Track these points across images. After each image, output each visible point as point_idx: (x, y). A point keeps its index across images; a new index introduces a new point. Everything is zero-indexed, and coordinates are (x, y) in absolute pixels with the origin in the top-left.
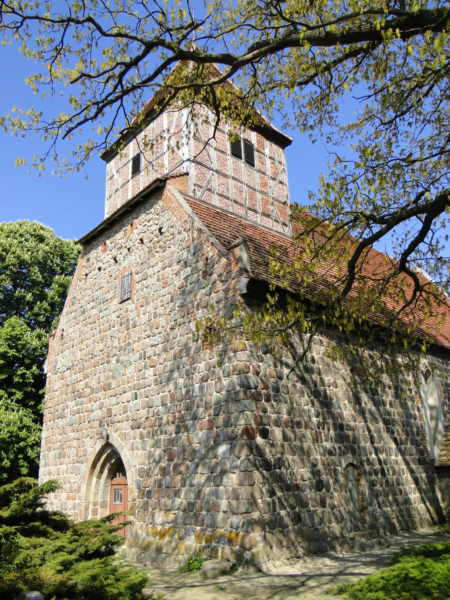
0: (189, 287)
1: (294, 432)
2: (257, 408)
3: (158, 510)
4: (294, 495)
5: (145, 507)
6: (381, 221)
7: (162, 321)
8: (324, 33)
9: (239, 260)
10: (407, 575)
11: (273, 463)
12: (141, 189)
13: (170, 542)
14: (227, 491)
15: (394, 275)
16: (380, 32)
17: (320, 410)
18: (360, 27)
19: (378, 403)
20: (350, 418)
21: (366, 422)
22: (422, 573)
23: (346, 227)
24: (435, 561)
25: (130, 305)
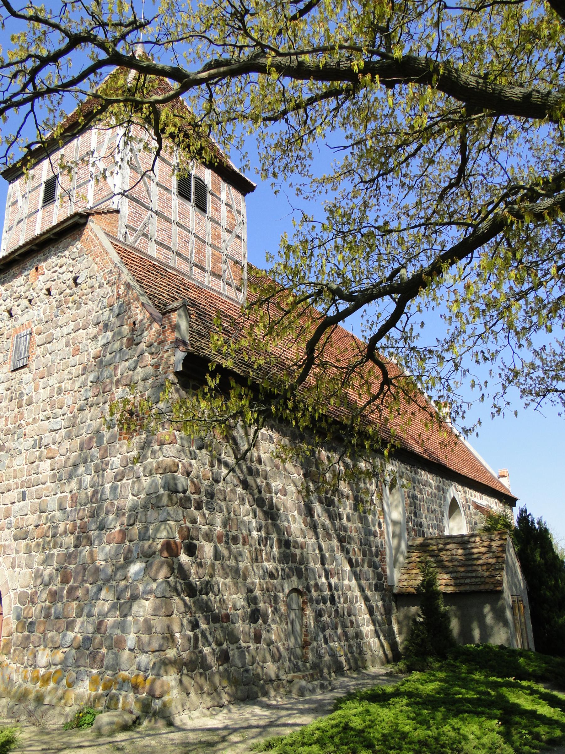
0: (108, 357)
1: (229, 549)
2: (184, 517)
3: (42, 647)
4: (222, 627)
5: (25, 644)
6: (349, 298)
7: (68, 399)
8: (296, 63)
9: (176, 327)
10: (347, 724)
11: (199, 587)
12: (54, 223)
13: (56, 689)
14: (136, 622)
15: (361, 363)
16: (357, 74)
17: (263, 523)
18: (338, 63)
19: (334, 516)
20: (298, 533)
21: (317, 538)
22: (364, 722)
23: (309, 300)
24: (382, 706)
25: (25, 375)
